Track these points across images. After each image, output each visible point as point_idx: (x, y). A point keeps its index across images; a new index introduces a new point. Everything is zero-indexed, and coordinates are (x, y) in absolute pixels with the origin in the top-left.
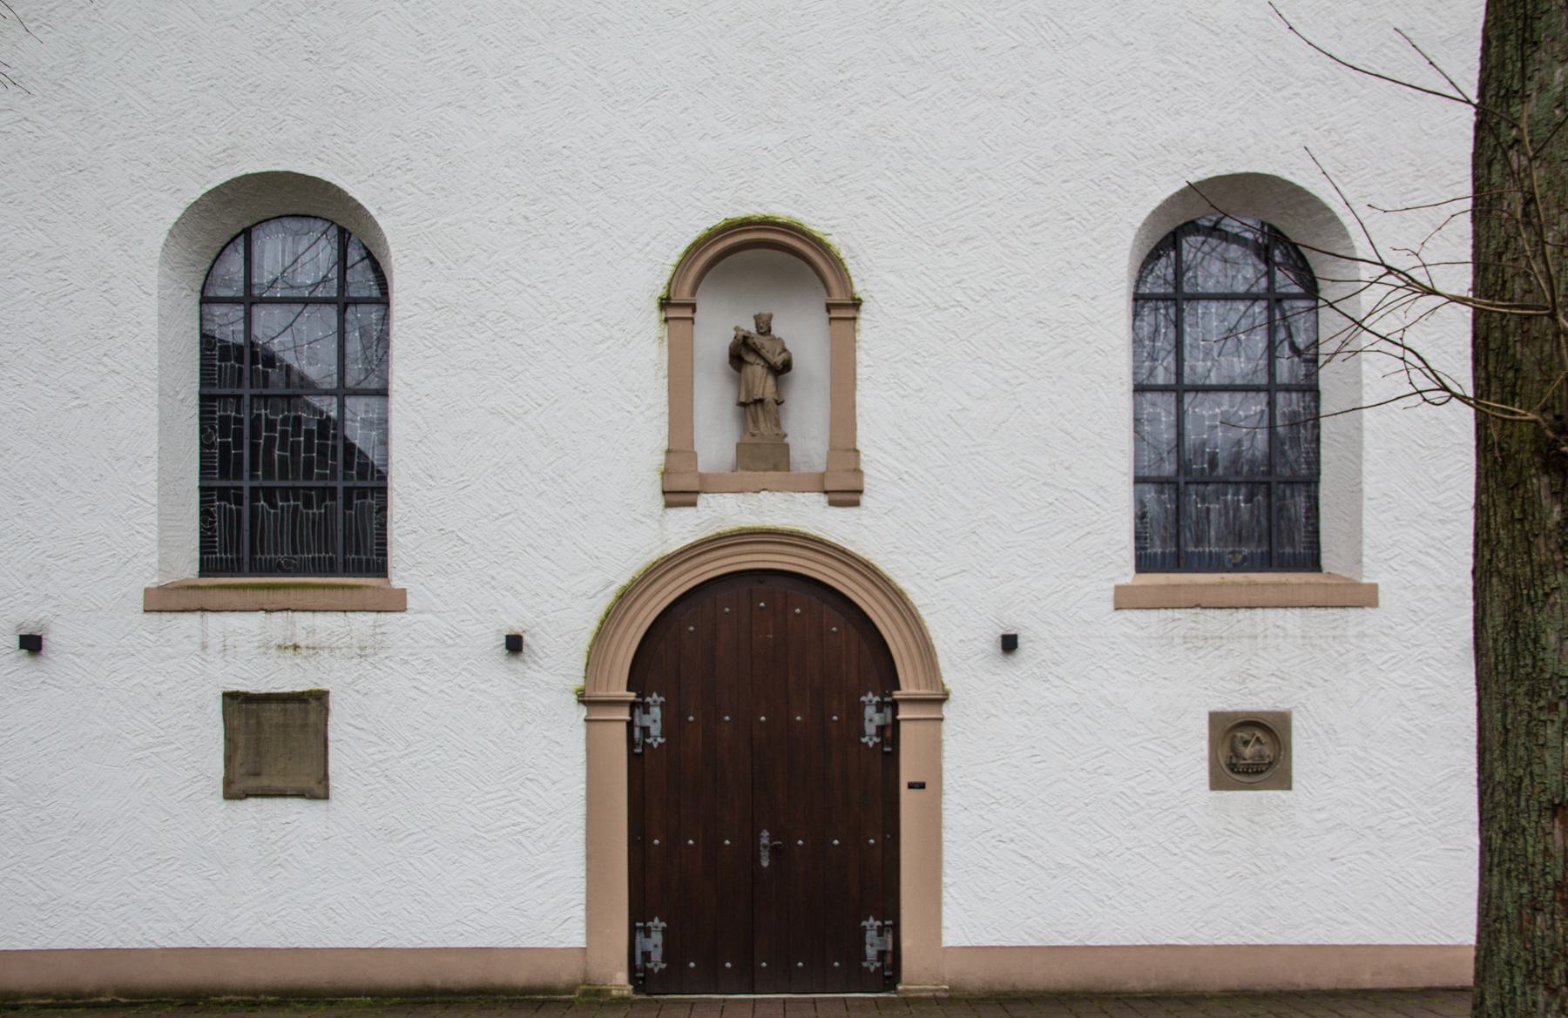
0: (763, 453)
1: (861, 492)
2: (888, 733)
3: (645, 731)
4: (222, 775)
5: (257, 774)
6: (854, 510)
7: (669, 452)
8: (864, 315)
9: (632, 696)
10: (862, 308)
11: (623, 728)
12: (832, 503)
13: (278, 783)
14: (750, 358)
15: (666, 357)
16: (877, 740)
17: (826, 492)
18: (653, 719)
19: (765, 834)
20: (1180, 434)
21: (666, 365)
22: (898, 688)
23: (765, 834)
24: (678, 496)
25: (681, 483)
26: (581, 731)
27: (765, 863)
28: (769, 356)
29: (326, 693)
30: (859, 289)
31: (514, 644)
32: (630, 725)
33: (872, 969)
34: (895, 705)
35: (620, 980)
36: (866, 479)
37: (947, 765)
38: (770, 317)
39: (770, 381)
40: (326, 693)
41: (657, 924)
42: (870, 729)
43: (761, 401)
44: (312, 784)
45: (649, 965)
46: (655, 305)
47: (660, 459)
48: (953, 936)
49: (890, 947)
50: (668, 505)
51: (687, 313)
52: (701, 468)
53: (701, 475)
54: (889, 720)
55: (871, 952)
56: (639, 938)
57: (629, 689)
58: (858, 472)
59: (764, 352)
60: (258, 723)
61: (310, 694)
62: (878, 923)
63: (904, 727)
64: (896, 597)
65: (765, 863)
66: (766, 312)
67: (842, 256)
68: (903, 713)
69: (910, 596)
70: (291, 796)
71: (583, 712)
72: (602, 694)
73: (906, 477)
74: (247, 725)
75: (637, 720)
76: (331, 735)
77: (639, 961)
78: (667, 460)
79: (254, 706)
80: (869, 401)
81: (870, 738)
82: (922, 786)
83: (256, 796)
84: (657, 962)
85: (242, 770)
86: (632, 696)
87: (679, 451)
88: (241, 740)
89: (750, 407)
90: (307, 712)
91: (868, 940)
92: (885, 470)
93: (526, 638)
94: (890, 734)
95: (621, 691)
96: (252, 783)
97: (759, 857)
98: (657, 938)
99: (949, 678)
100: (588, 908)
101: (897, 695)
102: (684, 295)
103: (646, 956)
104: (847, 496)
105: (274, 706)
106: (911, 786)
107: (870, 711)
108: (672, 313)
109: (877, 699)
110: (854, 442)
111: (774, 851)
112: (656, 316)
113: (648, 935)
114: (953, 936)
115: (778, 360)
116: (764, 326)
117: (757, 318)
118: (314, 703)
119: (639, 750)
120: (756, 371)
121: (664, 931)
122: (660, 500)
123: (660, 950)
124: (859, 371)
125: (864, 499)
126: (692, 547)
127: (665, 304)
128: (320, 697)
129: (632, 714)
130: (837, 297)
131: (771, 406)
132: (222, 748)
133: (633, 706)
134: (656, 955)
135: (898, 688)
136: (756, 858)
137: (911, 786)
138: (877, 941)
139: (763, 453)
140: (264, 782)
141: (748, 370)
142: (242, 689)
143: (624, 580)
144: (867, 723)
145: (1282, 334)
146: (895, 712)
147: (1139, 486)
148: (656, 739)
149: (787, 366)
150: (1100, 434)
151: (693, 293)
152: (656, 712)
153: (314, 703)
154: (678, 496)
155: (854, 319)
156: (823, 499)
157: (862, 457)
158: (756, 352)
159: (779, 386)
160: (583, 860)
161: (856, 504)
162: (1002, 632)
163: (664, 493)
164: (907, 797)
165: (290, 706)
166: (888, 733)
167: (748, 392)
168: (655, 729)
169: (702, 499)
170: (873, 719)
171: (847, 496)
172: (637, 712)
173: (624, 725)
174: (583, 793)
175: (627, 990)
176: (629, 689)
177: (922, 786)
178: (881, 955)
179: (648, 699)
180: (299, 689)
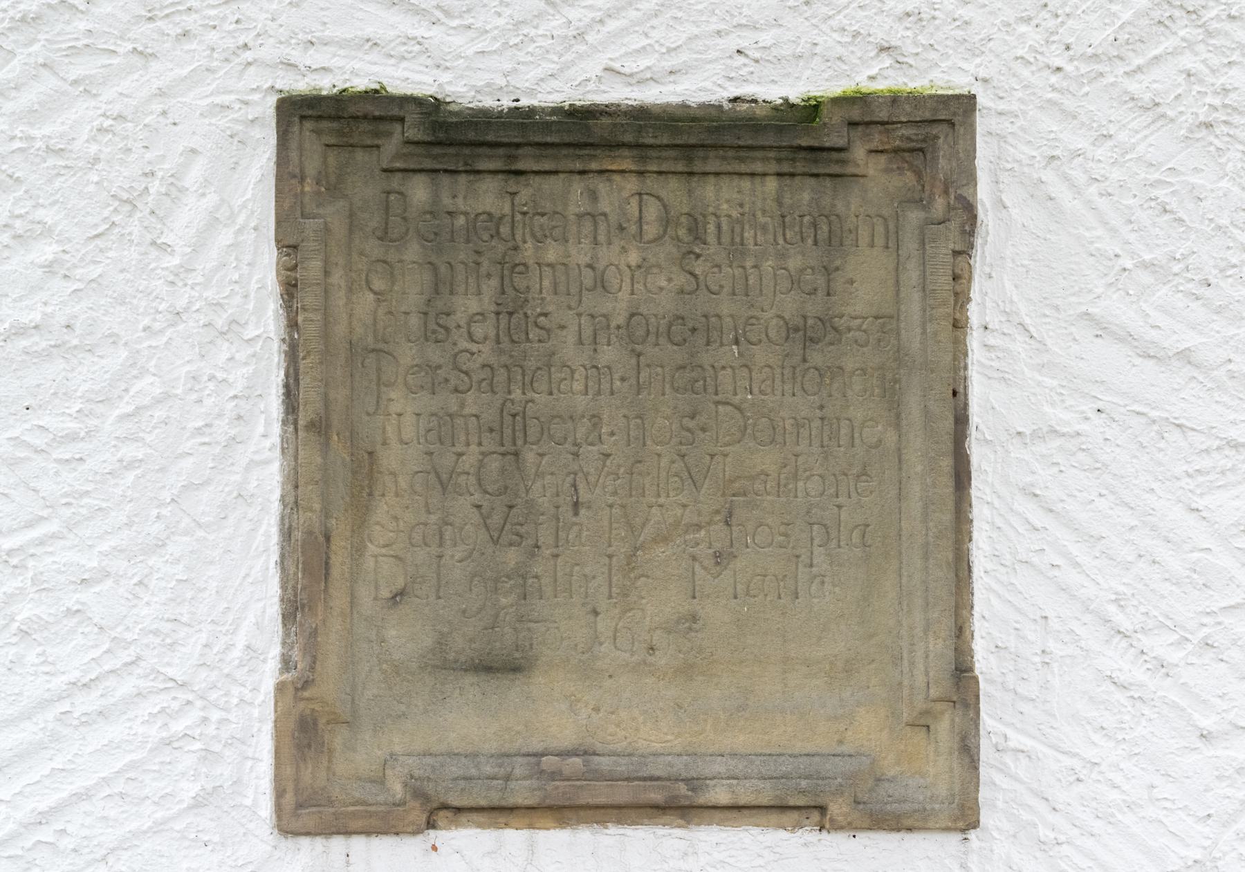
4: (269, 673)
5: (502, 665)
13: (644, 727)
20: (417, 143)
29: (954, 113)
40: (954, 113)
44: (869, 732)
60: (513, 311)
61: (861, 112)
70: (736, 811)
74: (436, 324)
76: (979, 393)
79: (487, 196)
83: (499, 813)
85: (406, 637)
88: (401, 423)
90: (831, 239)
96: (472, 724)
105: (617, 194)
118: (875, 177)
128: (924, 137)
132: (270, 480)
140: (550, 713)
142: (408, 78)
145: (892, 226)
153: (875, 177)
165: (723, 197)
180: (779, 87)
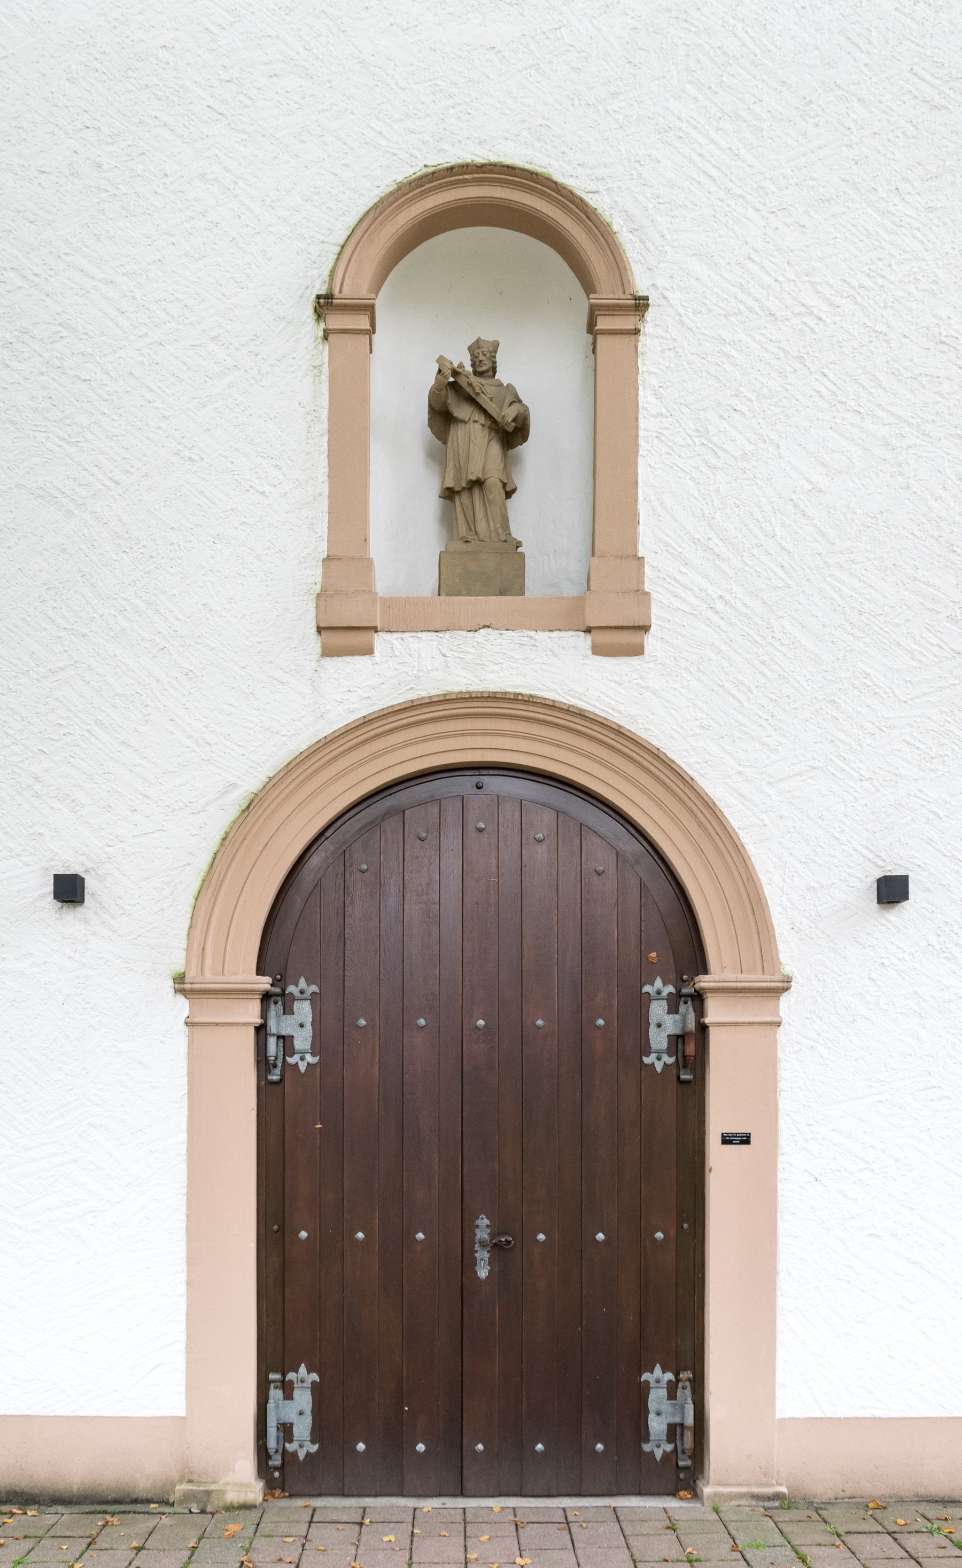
0: (481, 561)
1: (646, 628)
2: (690, 1049)
3: (286, 1041)
6: (633, 661)
7: (328, 560)
8: (651, 324)
9: (265, 983)
10: (650, 315)
11: (248, 1038)
12: (598, 650)
14: (462, 411)
15: (325, 401)
16: (670, 1060)
17: (588, 630)
18: (299, 1024)
19: (484, 1221)
21: (324, 414)
22: (705, 971)
23: (484, 1221)
24: (344, 634)
25: (349, 614)
26: (180, 1039)
27: (483, 1273)
28: (492, 408)
30: (641, 284)
31: (69, 890)
32: (261, 1030)
33: (658, 1454)
34: (698, 999)
35: (240, 1478)
36: (655, 610)
37: (785, 1104)
38: (496, 345)
39: (496, 448)
41: (304, 1376)
42: (658, 1039)
43: (478, 483)
45: (290, 1447)
46: (308, 311)
47: (314, 576)
48: (789, 1404)
49: (690, 1421)
50: (328, 652)
51: (363, 322)
52: (380, 595)
53: (383, 600)
54: (691, 1026)
55: (657, 1425)
56: (275, 1394)
57: (260, 971)
58: (643, 597)
59: (483, 400)
62: (669, 1376)
63: (715, 1036)
64: (704, 813)
65: (483, 1273)
66: (488, 337)
67: (615, 228)
68: (715, 1012)
69: (727, 812)
71: (182, 1006)
72: (210, 979)
73: (719, 606)
75: (273, 1026)
77: (272, 1443)
78: (326, 576)
80: (661, 474)
81: (659, 1060)
82: (745, 1140)
84: (303, 1444)
86: (265, 983)
87: (345, 560)
89: (464, 496)
91: (652, 1405)
92: (690, 597)
93: (90, 884)
94: (692, 1049)
95: (243, 969)
97: (474, 1262)
98: (303, 1399)
99: (790, 955)
100: (189, 1349)
101: (704, 982)
102: (354, 287)
103: (286, 1430)
104: (621, 636)
106: (727, 1140)
107: (658, 1010)
108: (336, 321)
109: (670, 989)
110: (634, 543)
111: (497, 1248)
112: (311, 329)
113: (288, 1396)
114: (789, 1404)
115: (509, 414)
116: (484, 360)
117: (475, 349)
119: (275, 1077)
120: (473, 436)
121: (315, 1387)
122: (314, 643)
123: (308, 1420)
124: (642, 423)
125: (650, 641)
126: (366, 722)
127: (325, 304)
129: (264, 1014)
130: (606, 294)
131: (495, 492)
133: (266, 997)
134: (303, 1428)
135: (705, 971)
136: (467, 1262)
137: (727, 1140)
138: (666, 1406)
139: (481, 561)
141: (458, 434)
143: (253, 782)
144: (653, 1030)
146: (700, 1012)
147: (469, 1485)
148: (304, 1060)
149: (514, 491)
150: (878, 790)
151: (377, 287)
152: (304, 1010)
154: (344, 634)
155: (637, 332)
156: (585, 641)
157: (648, 571)
158: (471, 400)
159: (509, 463)
160: (183, 1267)
161: (637, 651)
162: (879, 874)
163: (319, 630)
164: (718, 1157)
166: (690, 1049)
167: (458, 470)
168: (303, 1040)
169: (381, 641)
170: (663, 1024)
171: (621, 636)
172: (273, 1010)
173: (251, 1032)
174: (183, 1149)
175: (254, 1491)
176: (260, 971)
177: (745, 1140)
178: (674, 1431)
179: (291, 989)
